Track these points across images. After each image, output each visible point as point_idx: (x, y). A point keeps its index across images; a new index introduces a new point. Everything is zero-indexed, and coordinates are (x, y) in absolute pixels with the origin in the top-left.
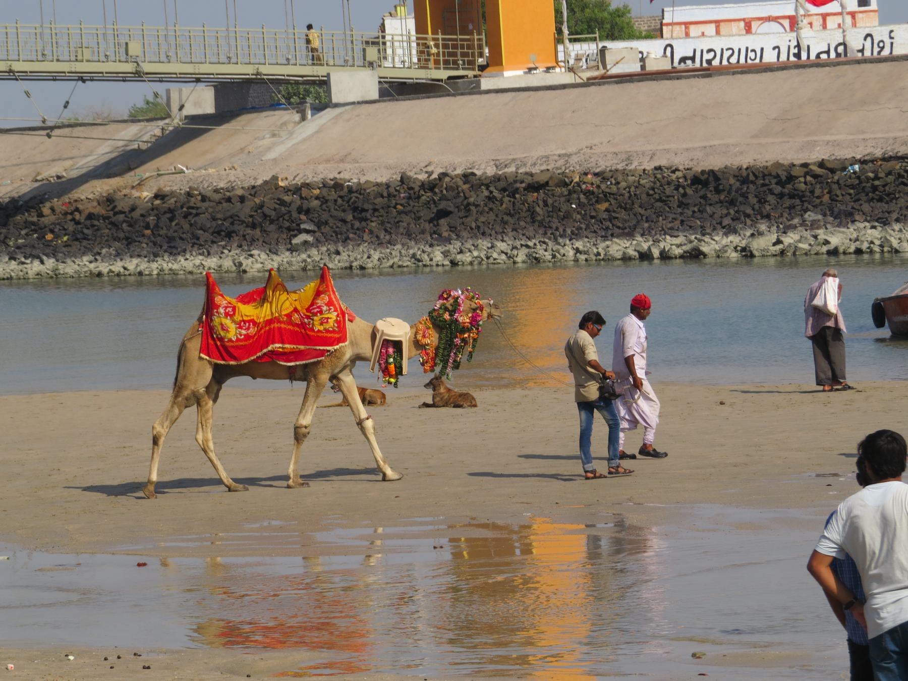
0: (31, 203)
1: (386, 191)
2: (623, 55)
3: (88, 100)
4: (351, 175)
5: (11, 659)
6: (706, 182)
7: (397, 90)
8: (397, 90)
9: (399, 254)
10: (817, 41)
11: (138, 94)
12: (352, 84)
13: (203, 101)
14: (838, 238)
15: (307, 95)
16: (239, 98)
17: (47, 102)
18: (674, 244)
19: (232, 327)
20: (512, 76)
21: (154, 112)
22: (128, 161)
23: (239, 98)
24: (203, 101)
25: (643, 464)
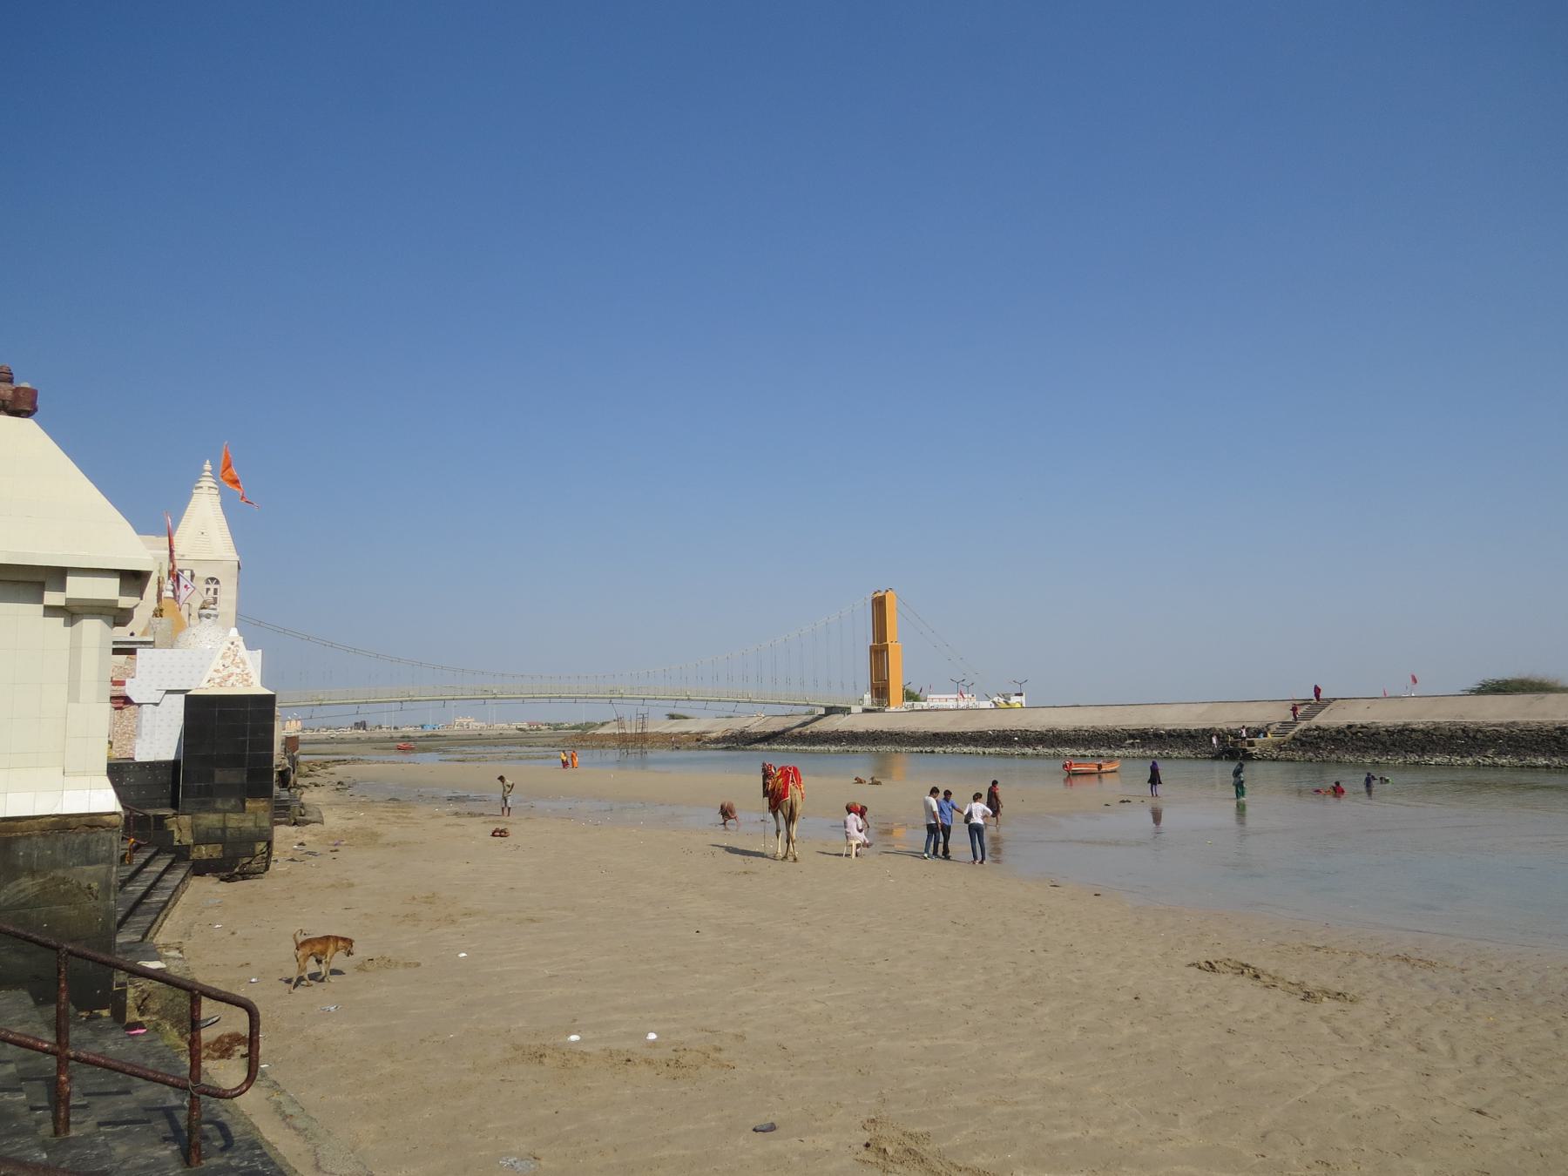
0: (783, 732)
1: (1426, 733)
2: (918, 705)
3: (796, 710)
4: (855, 730)
5: (653, 1043)
6: (936, 735)
7: (866, 711)
8: (866, 711)
9: (865, 748)
10: (962, 704)
11: (807, 709)
12: (856, 709)
13: (823, 711)
14: (966, 750)
15: (846, 711)
16: (830, 711)
17: (787, 710)
18: (928, 749)
19: (261, 813)
20: (892, 709)
21: (811, 713)
22: (804, 724)
23: (830, 711)
24: (823, 711)
25: (334, 979)
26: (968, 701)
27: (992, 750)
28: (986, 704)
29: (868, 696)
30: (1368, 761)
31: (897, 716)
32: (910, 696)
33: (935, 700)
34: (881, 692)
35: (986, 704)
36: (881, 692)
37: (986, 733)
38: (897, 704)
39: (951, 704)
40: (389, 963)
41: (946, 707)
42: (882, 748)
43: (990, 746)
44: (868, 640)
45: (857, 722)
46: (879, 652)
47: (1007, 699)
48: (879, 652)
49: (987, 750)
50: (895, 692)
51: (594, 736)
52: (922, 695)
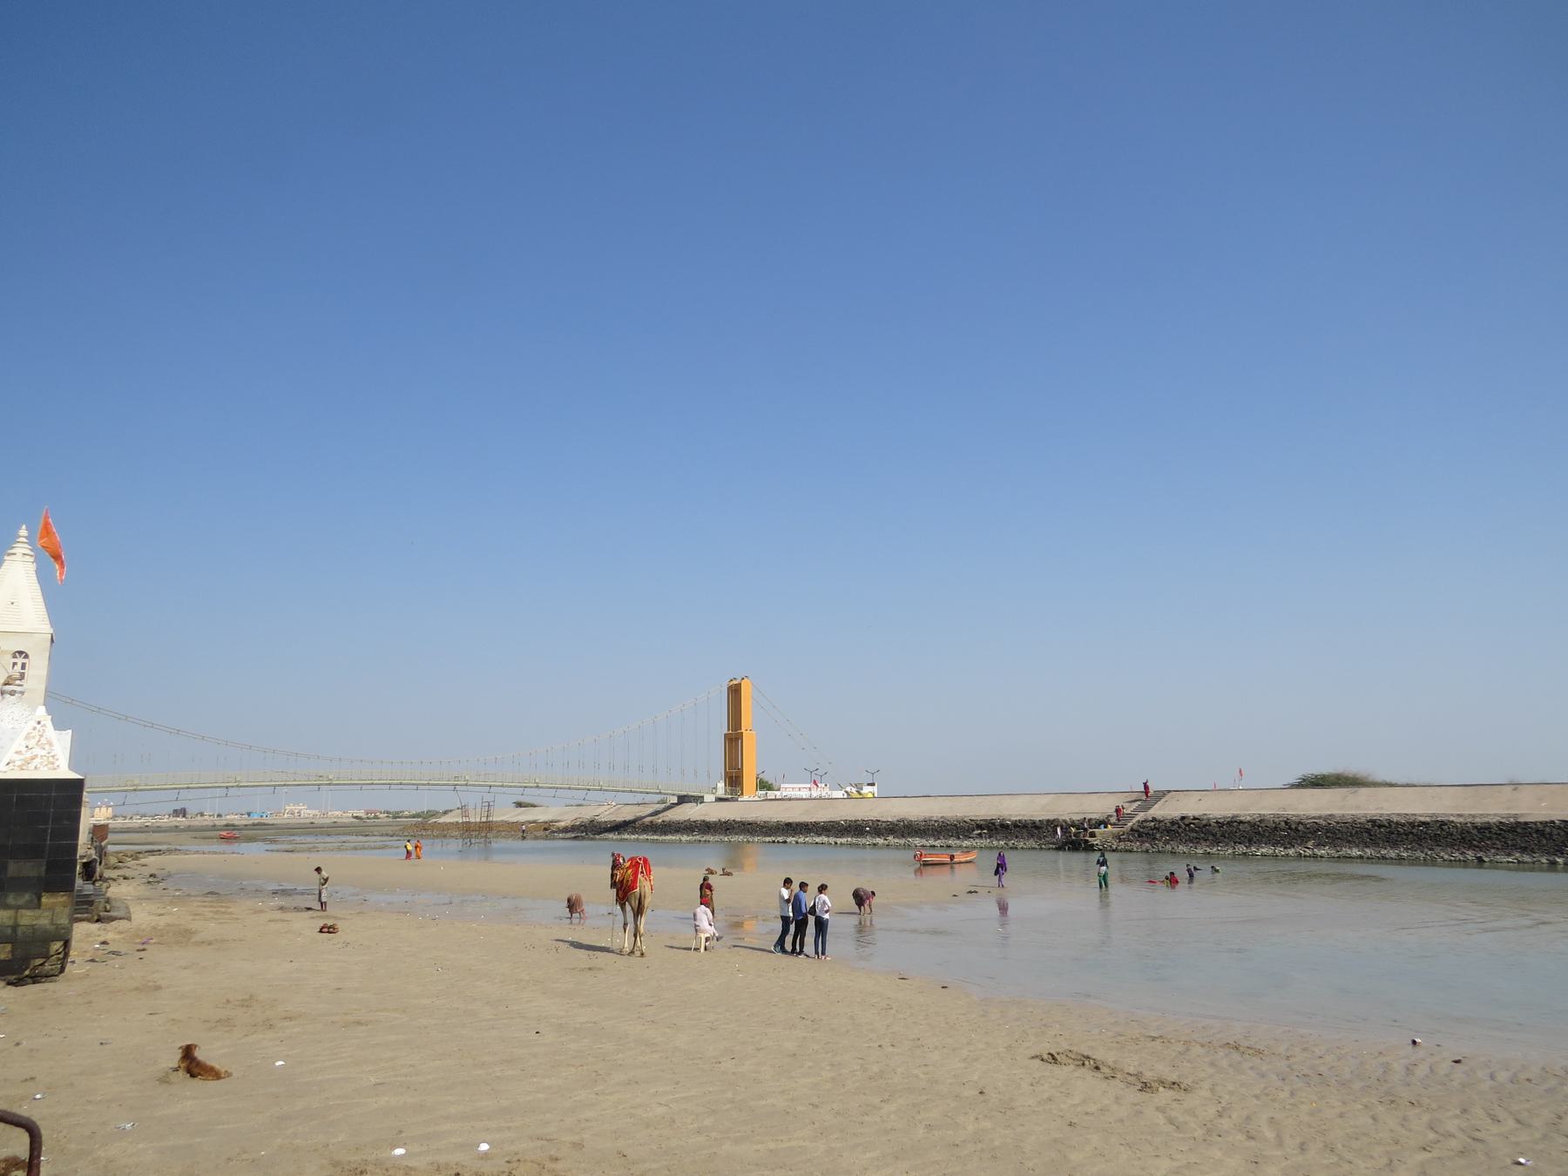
2: (771, 795)
6: (789, 825)
7: (719, 800)
8: (719, 800)
9: (717, 838)
10: (815, 794)
12: (709, 798)
20: (745, 798)
26: (822, 791)
27: (843, 840)
28: (839, 794)
29: (721, 785)
32: (764, 785)
34: (734, 780)
35: (839, 794)
36: (734, 780)
37: (838, 823)
38: (750, 793)
39: (804, 794)
40: (1293, 786)
42: (735, 838)
46: (733, 740)
47: (859, 788)
48: (733, 740)
49: (839, 841)
50: (749, 781)
52: (775, 786)
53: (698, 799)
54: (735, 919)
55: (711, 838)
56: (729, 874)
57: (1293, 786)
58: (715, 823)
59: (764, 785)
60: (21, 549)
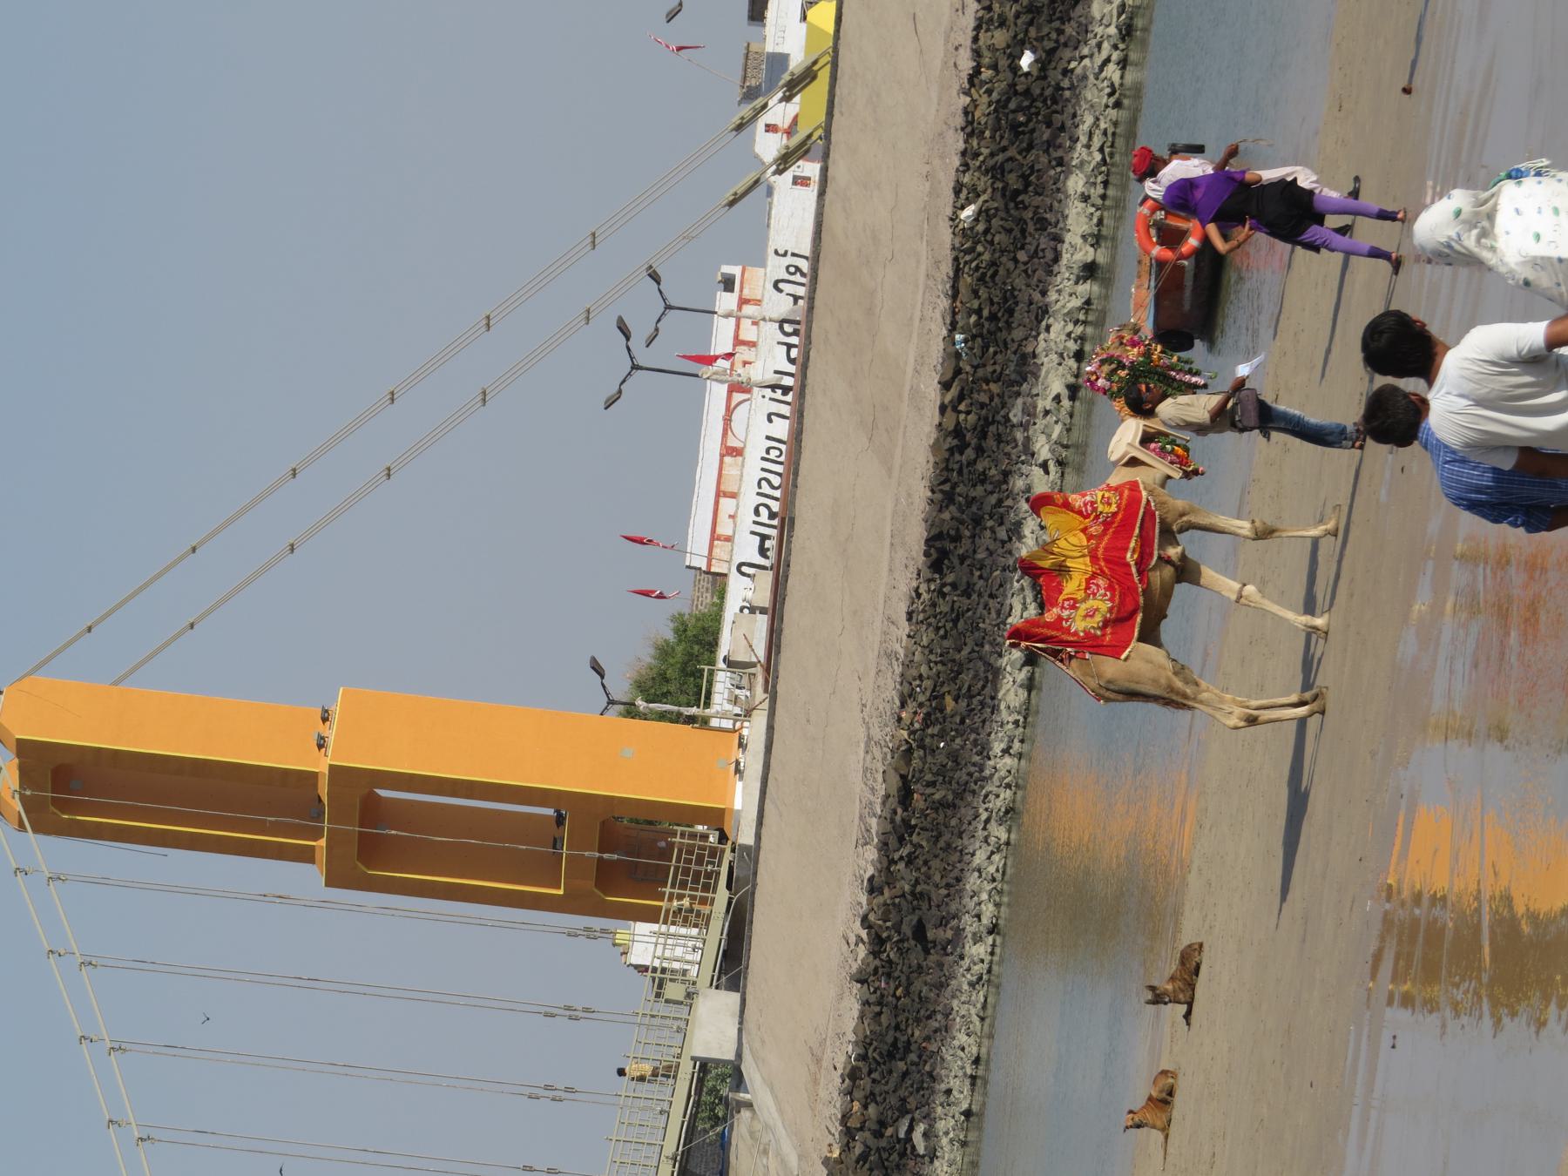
2: (741, 636)
4: (842, 1053)
6: (941, 551)
7: (732, 965)
8: (732, 965)
9: (965, 1005)
10: (770, 359)
12: (713, 1028)
20: (741, 799)
26: (752, 331)
27: (1077, 221)
28: (792, 212)
29: (644, 942)
30: (1175, 359)
31: (794, 783)
32: (679, 676)
33: (723, 522)
34: (627, 857)
35: (792, 212)
36: (627, 857)
37: (967, 242)
38: (714, 769)
39: (761, 424)
40: (1283, 898)
41: (774, 460)
42: (980, 899)
43: (1049, 227)
44: (288, 893)
45: (794, 1029)
46: (378, 833)
47: (769, 78)
48: (378, 833)
49: (1075, 251)
50: (639, 765)
51: (1170, 377)
52: (686, 600)
53: (716, 1094)
54: (1384, 894)
55: (961, 1044)
56: (1190, 967)
57: (1283, 898)
58: (874, 1007)
59: (679, 676)
60: (1544, 324)
